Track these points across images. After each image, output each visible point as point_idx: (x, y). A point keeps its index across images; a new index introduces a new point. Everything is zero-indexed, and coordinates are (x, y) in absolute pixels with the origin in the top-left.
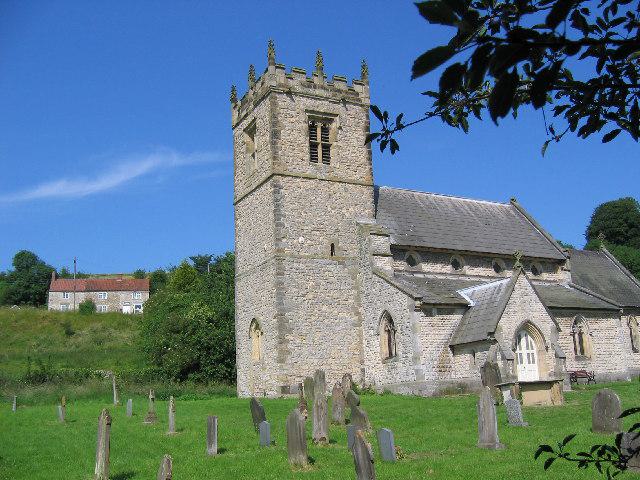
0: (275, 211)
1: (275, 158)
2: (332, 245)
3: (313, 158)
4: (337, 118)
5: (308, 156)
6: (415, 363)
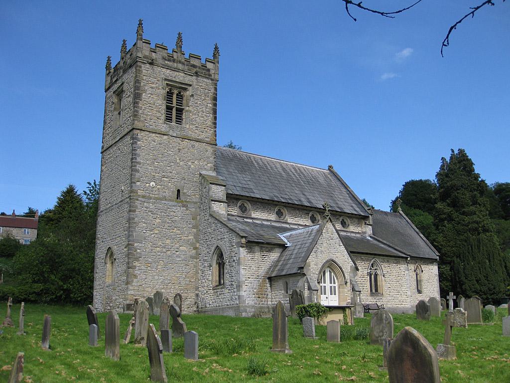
2: (179, 191)
3: (169, 119)
4: (190, 88)
5: (163, 117)
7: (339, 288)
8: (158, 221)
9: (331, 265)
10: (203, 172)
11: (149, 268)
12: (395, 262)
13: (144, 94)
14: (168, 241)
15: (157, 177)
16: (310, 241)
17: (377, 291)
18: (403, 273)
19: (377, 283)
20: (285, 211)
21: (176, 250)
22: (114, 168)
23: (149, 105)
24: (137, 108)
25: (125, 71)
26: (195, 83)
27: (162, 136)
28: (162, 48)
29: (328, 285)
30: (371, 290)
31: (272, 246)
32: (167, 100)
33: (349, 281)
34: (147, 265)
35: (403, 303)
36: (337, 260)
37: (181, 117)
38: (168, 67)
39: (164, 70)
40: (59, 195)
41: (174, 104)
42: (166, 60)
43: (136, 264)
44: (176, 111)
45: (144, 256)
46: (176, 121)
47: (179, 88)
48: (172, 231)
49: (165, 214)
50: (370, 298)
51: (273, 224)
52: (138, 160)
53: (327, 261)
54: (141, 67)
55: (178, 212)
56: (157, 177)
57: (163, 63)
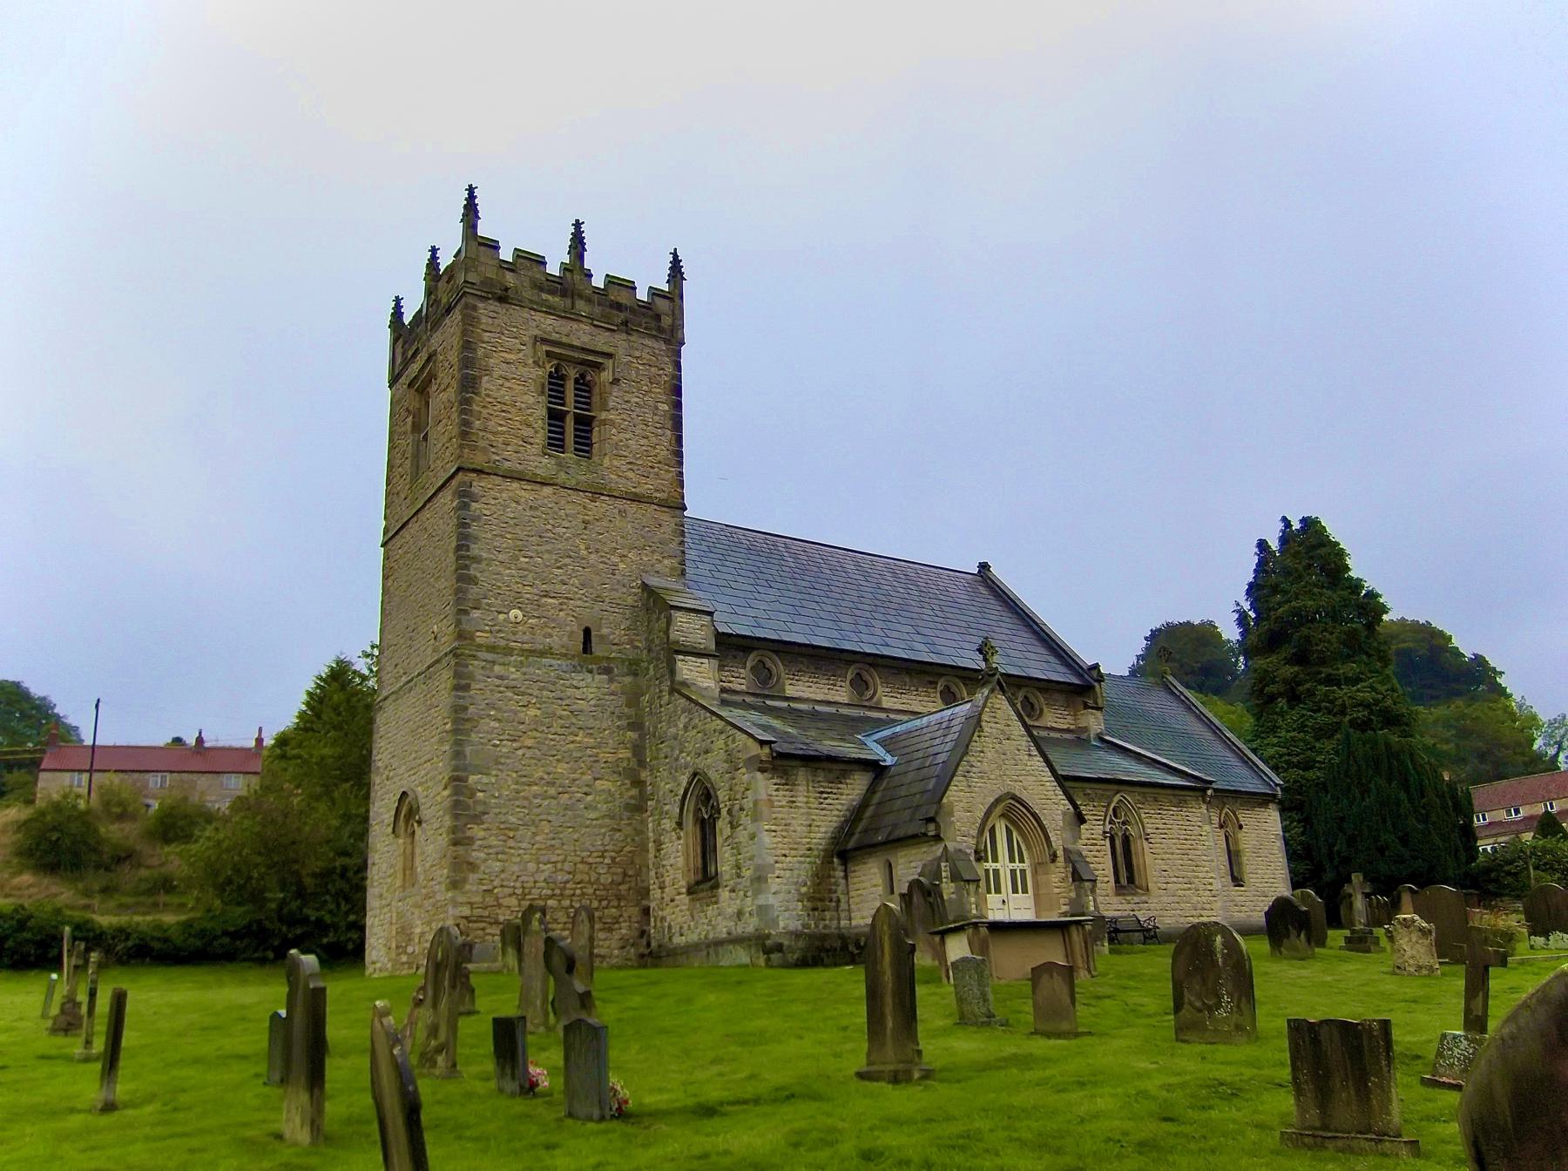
0: (459, 548)
1: (464, 435)
2: (587, 632)
3: (556, 442)
4: (609, 363)
5: (541, 438)
6: (757, 893)
7: (1035, 873)
8: (532, 712)
9: (1013, 809)
10: (653, 581)
11: (511, 843)
12: (1175, 801)
13: (485, 379)
14: (561, 768)
15: (528, 596)
16: (949, 746)
17: (1133, 883)
18: (1197, 830)
19: (1131, 858)
20: (875, 679)
21: (585, 789)
22: (415, 578)
23: (499, 406)
24: (466, 415)
25: (436, 325)
26: (621, 351)
27: (537, 487)
28: (530, 259)
29: (1004, 865)
30: (1117, 881)
31: (843, 766)
32: (550, 396)
33: (1060, 853)
34: (505, 835)
35: (1202, 912)
36: (1024, 796)
37: (588, 438)
38: (549, 307)
39: (538, 316)
40: (310, 685)
41: (570, 406)
42: (542, 290)
43: (477, 831)
44: (575, 423)
45: (497, 810)
46: (576, 449)
47: (581, 364)
48: (571, 738)
49: (551, 695)
50: (1116, 899)
51: (844, 711)
52: (475, 550)
53: (998, 801)
54: (475, 308)
55: (589, 688)
56: (528, 596)
57: (535, 298)
